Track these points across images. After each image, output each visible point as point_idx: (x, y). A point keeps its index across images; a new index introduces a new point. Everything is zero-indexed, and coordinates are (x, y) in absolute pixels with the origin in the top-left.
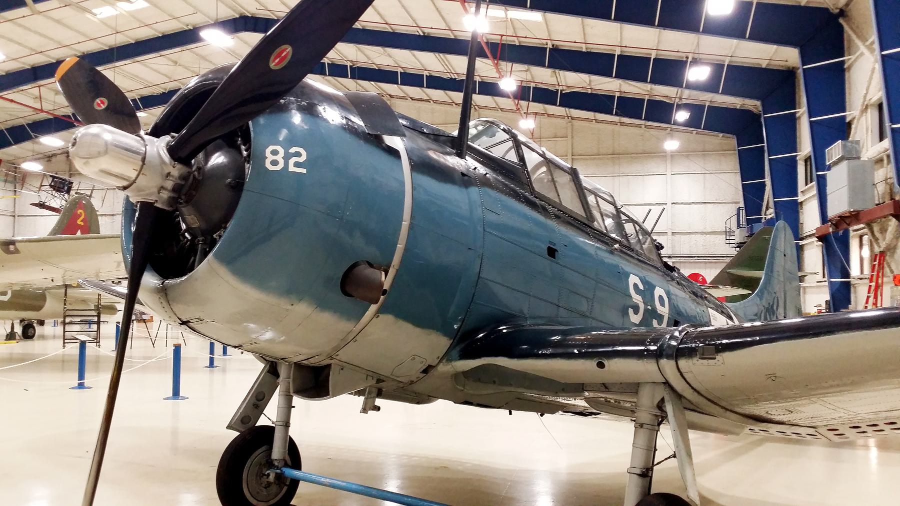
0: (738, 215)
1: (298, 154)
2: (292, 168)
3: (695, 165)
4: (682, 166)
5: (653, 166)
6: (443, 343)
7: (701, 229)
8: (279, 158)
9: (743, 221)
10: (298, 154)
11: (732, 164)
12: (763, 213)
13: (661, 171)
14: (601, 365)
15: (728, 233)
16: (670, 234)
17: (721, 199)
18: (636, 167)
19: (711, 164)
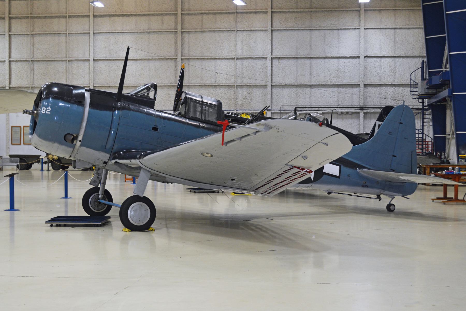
0: (422, 68)
1: (49, 109)
2: (47, 113)
3: (387, 20)
4: (373, 20)
5: (349, 20)
6: (108, 156)
7: (390, 81)
8: (44, 110)
9: (426, 75)
10: (49, 109)
11: (418, 19)
12: (444, 66)
13: (356, 25)
14: (80, 141)
15: (413, 86)
16: (362, 86)
17: (410, 54)
18: (331, 22)
19: (401, 20)
